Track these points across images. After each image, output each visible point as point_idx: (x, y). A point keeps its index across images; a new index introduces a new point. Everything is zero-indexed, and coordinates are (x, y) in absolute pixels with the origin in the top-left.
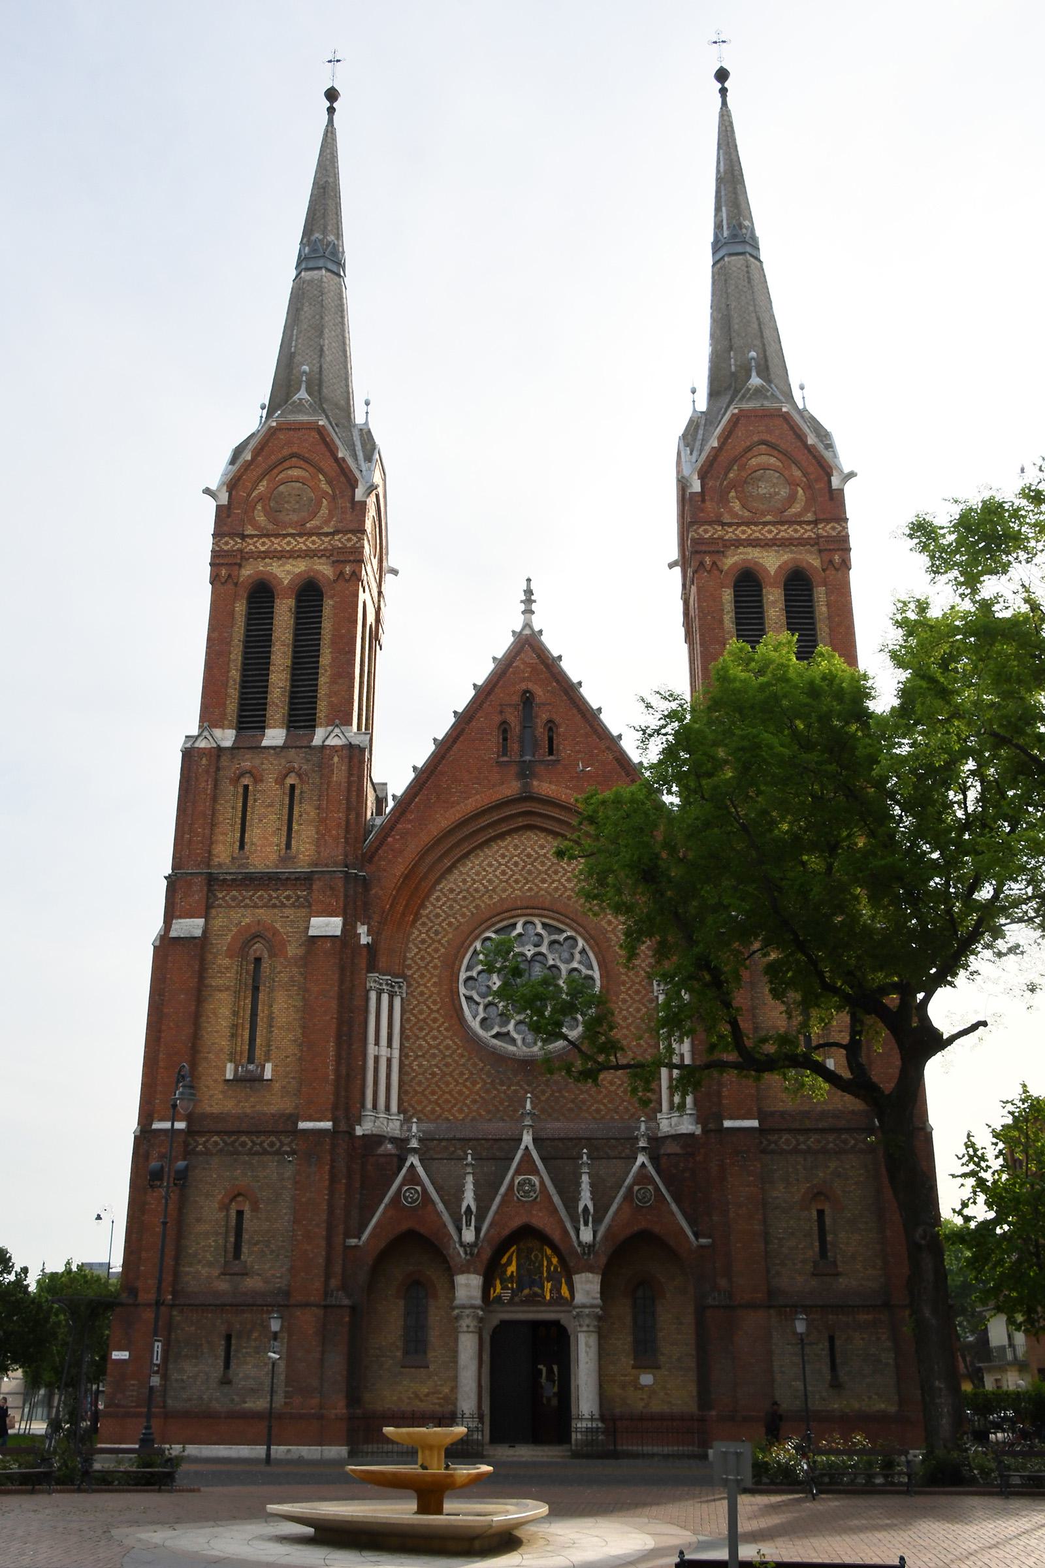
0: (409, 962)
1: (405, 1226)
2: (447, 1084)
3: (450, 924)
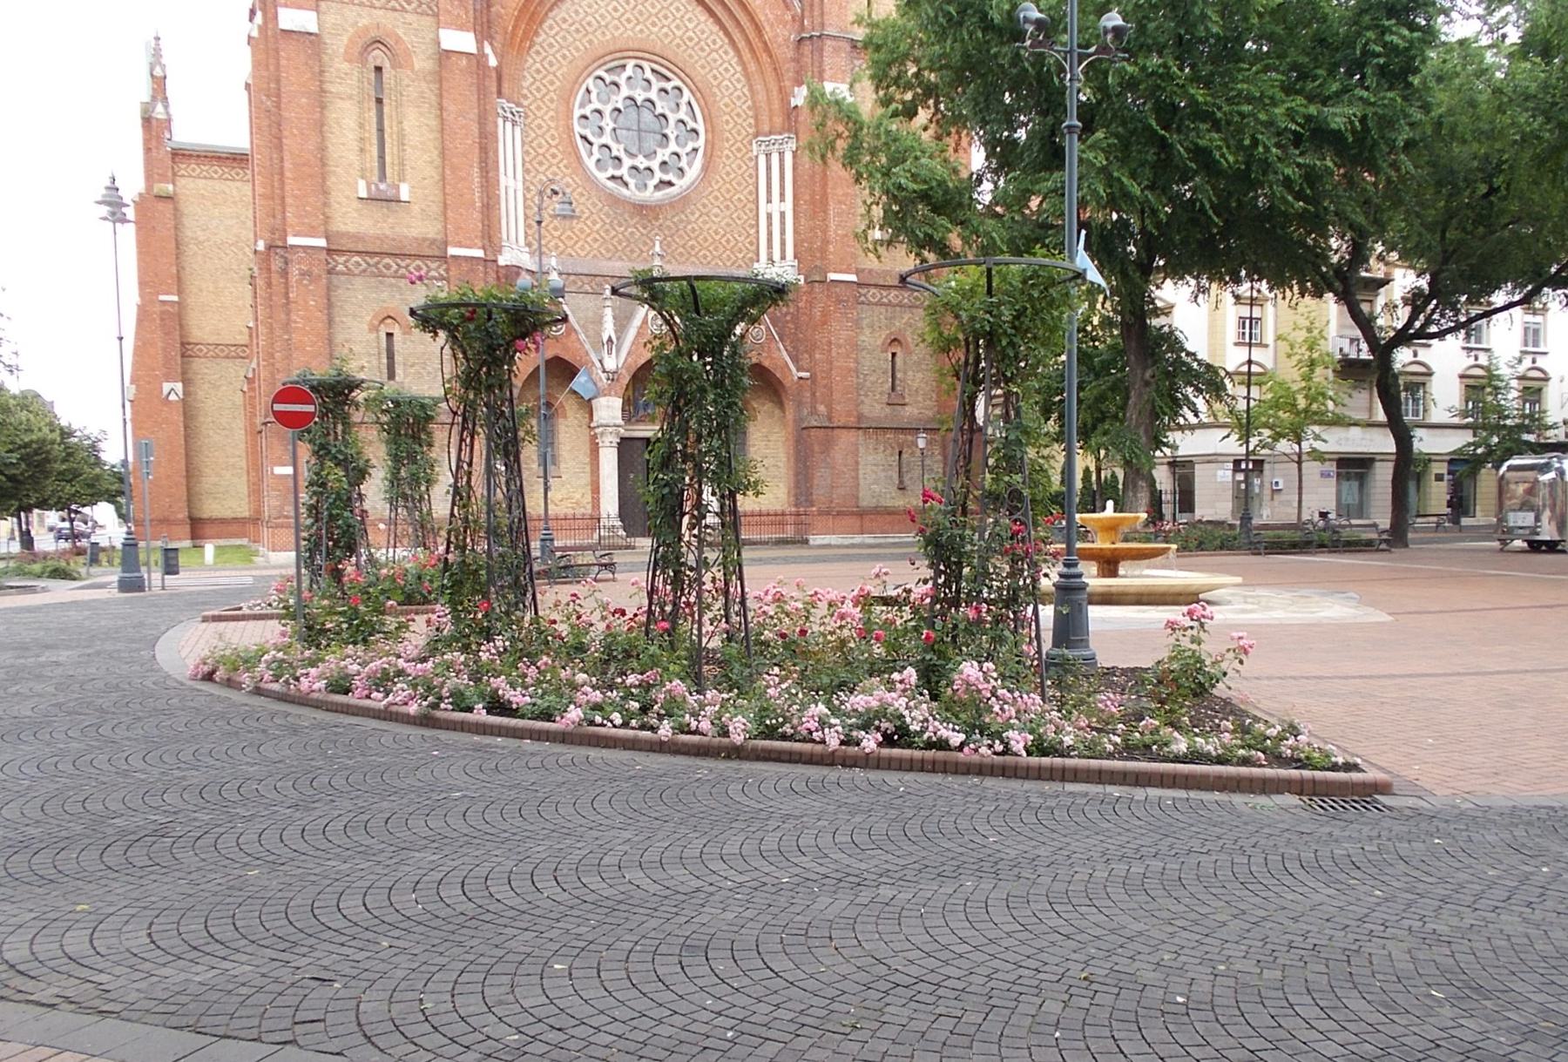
0: (525, 91)
3: (564, 57)
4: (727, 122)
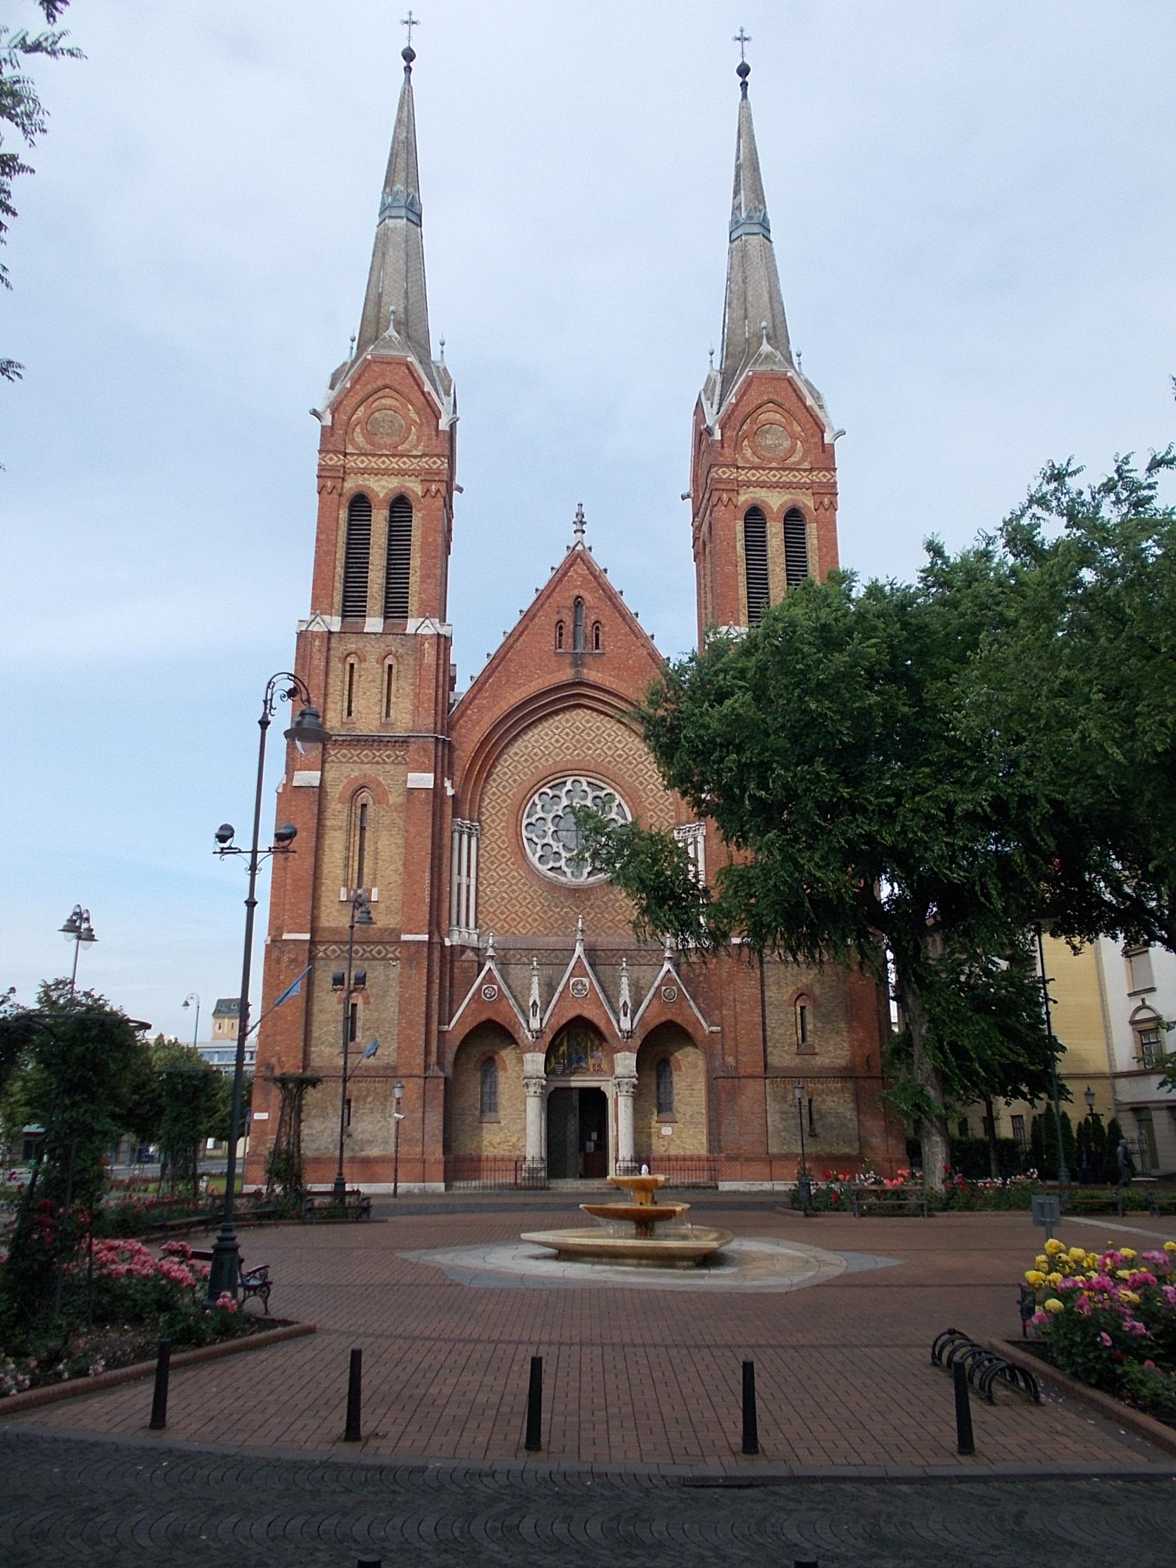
1: (483, 1017)
2: (514, 906)
3: (515, 781)
4: (652, 817)
